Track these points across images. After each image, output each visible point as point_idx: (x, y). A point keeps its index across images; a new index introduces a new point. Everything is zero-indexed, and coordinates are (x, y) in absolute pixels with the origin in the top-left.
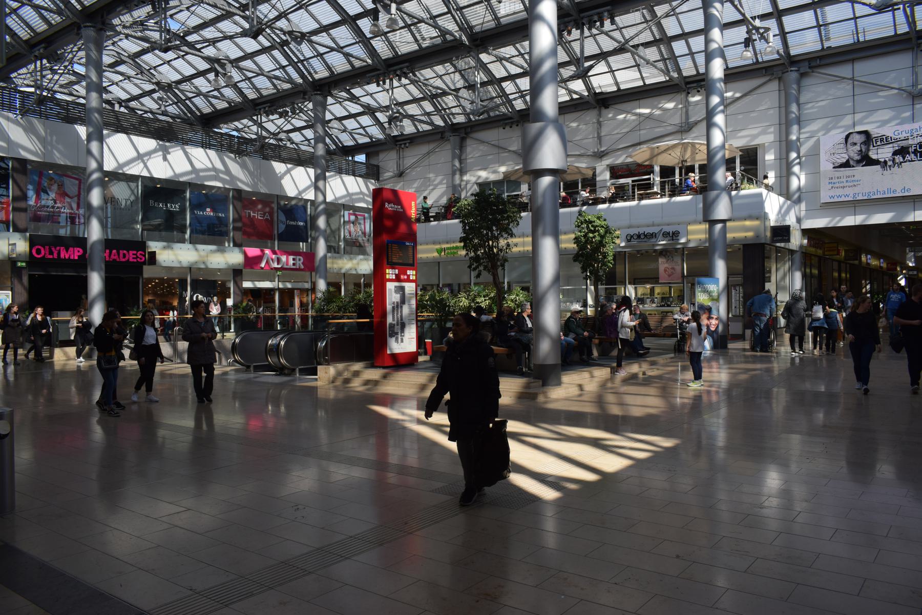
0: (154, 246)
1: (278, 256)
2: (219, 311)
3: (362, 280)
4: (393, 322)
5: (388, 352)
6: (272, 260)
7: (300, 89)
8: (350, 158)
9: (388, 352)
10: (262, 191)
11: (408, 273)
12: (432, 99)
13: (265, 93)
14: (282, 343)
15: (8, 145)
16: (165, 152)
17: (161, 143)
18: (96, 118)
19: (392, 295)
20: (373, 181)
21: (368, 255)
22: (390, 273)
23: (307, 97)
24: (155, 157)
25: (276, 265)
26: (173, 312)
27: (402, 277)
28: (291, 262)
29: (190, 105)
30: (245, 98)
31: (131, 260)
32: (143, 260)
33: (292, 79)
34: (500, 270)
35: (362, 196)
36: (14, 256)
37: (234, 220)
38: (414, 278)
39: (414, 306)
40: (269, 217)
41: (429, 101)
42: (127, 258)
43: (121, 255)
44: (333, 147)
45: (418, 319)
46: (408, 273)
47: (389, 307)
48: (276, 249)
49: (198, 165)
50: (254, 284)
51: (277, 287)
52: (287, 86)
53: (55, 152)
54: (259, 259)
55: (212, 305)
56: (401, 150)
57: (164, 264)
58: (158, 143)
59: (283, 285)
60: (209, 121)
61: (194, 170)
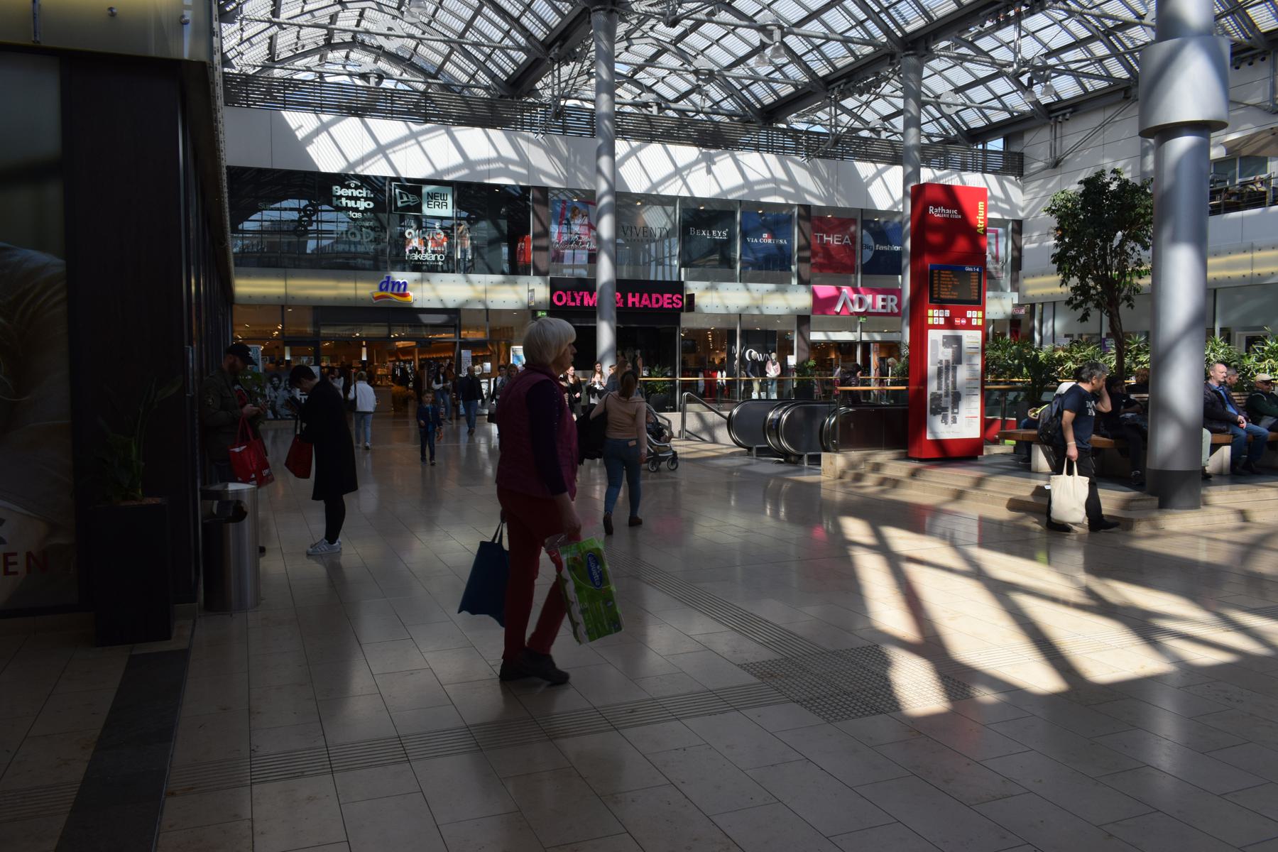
0: (694, 287)
1: (860, 296)
2: (779, 373)
3: (991, 329)
4: (939, 392)
5: (929, 437)
6: (852, 301)
7: (885, 51)
8: (980, 147)
9: (929, 437)
10: (840, 205)
11: (969, 316)
12: (1107, 36)
13: (839, 65)
14: (785, 417)
15: (528, 171)
16: (710, 161)
17: (704, 150)
18: (606, 125)
19: (937, 347)
20: (1013, 178)
21: (1002, 290)
22: (935, 316)
23: (895, 61)
24: (696, 170)
25: (857, 309)
26: (722, 373)
27: (957, 321)
28: (880, 303)
29: (748, 96)
30: (814, 76)
31: (666, 306)
32: (680, 306)
33: (874, 38)
34: (1123, 308)
35: (502, 165)
36: (533, 304)
37: (800, 249)
38: (980, 322)
39: (979, 367)
40: (849, 242)
41: (1102, 41)
42: (660, 304)
43: (654, 300)
44: (953, 132)
45: (986, 387)
46: (969, 316)
47: (931, 369)
48: (859, 285)
49: (752, 176)
50: (827, 336)
51: (858, 340)
52: (868, 50)
53: (580, 175)
54: (833, 300)
55: (769, 365)
56: (1058, 125)
57: (707, 311)
58: (701, 151)
59: (869, 336)
60: (772, 114)
61: (748, 183)
